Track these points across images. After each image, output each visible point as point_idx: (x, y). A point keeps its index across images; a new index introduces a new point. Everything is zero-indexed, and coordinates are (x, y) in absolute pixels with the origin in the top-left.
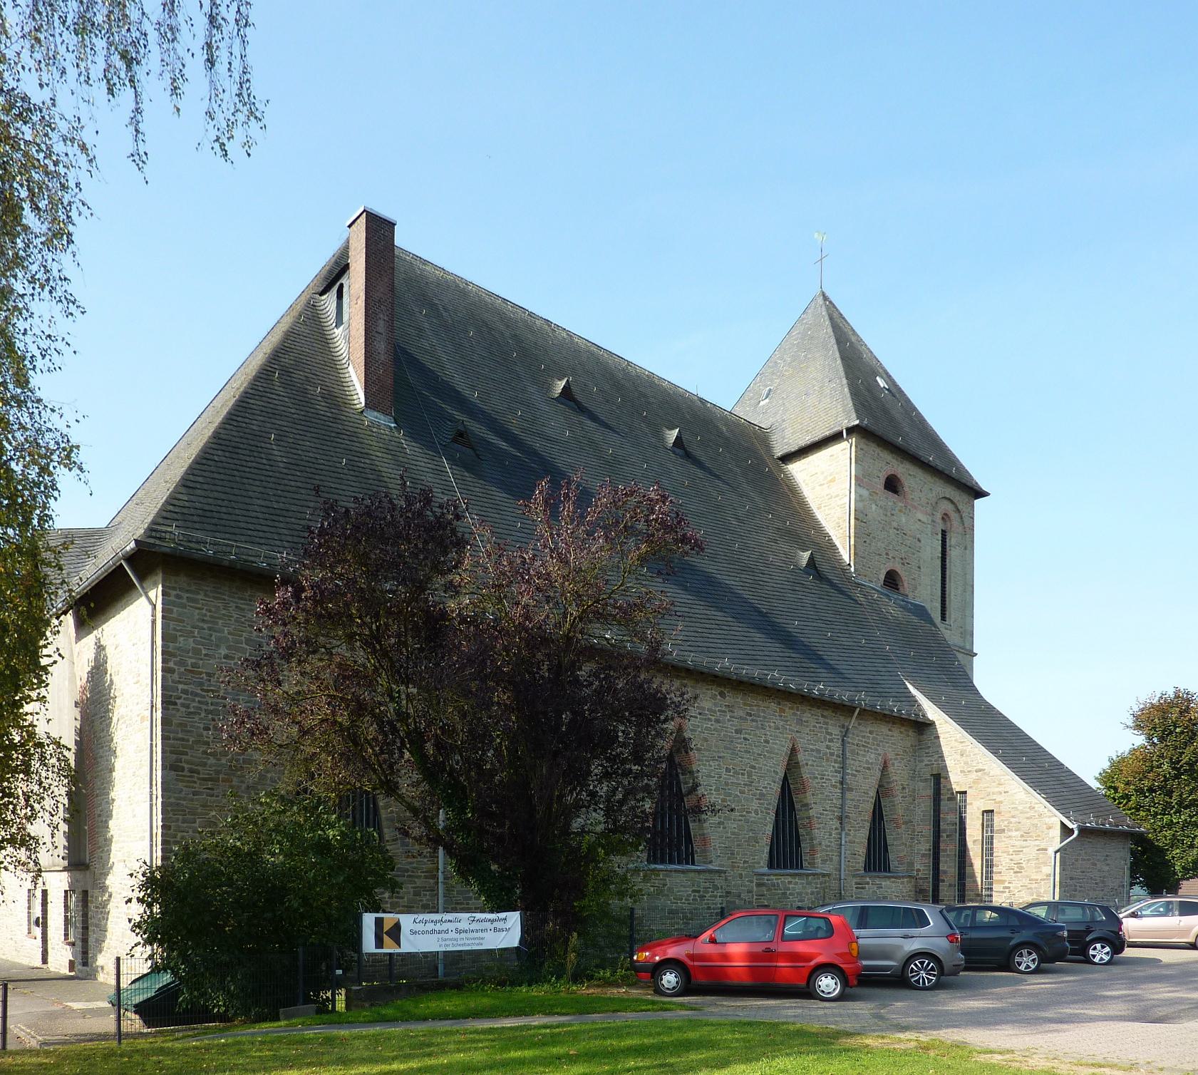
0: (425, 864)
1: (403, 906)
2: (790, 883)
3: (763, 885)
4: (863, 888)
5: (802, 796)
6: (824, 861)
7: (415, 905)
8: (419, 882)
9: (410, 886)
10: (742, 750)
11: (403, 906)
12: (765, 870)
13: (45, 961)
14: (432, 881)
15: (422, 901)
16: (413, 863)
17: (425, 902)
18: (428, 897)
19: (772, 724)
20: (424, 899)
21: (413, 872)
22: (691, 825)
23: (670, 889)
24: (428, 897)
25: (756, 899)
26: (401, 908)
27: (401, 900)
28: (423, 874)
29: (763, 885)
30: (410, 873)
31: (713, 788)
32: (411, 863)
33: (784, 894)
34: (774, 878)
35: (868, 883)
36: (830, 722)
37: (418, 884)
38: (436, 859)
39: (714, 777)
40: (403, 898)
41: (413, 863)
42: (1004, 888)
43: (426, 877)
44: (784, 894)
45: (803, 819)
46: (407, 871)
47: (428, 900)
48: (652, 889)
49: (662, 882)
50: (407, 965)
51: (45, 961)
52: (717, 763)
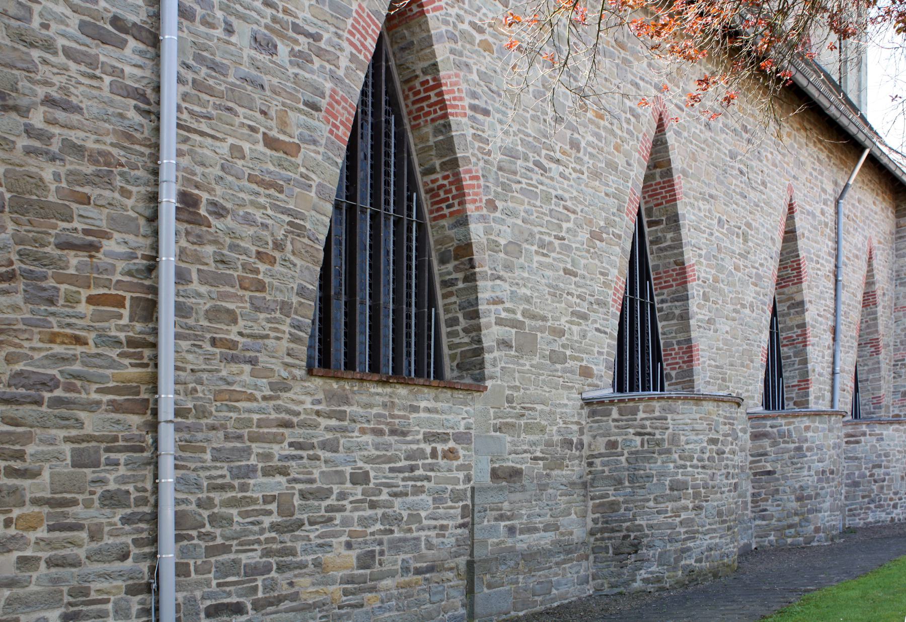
0: (112, 364)
1: (36, 502)
2: (807, 428)
3: (765, 435)
4: (858, 442)
5: (794, 289)
6: (817, 398)
7: (80, 497)
8: (91, 423)
9: (62, 433)
10: (738, 190)
11: (36, 502)
12: (760, 409)
13: (832, 407)
14: (135, 420)
15: (102, 481)
16: (73, 359)
17: (112, 486)
18: (122, 470)
19: (769, 156)
20: (111, 477)
21: (69, 388)
22: (660, 325)
23: (674, 440)
24: (122, 470)
25: (752, 462)
26: (29, 509)
27: (26, 483)
28: (106, 398)
29: (765, 435)
30: (58, 393)
31: (703, 252)
32: (64, 359)
33: (799, 449)
34: (783, 421)
35: (864, 434)
36: (826, 173)
37: (88, 430)
38: (147, 352)
39: (704, 232)
40: (35, 474)
41: (73, 359)
42: (330, 509)
43: (116, 407)
44: (799, 449)
45: (791, 329)
46: (49, 383)
47: (123, 480)
48: (638, 439)
49: (658, 423)
50: (67, 25)
51: (832, 407)
52: (707, 207)
